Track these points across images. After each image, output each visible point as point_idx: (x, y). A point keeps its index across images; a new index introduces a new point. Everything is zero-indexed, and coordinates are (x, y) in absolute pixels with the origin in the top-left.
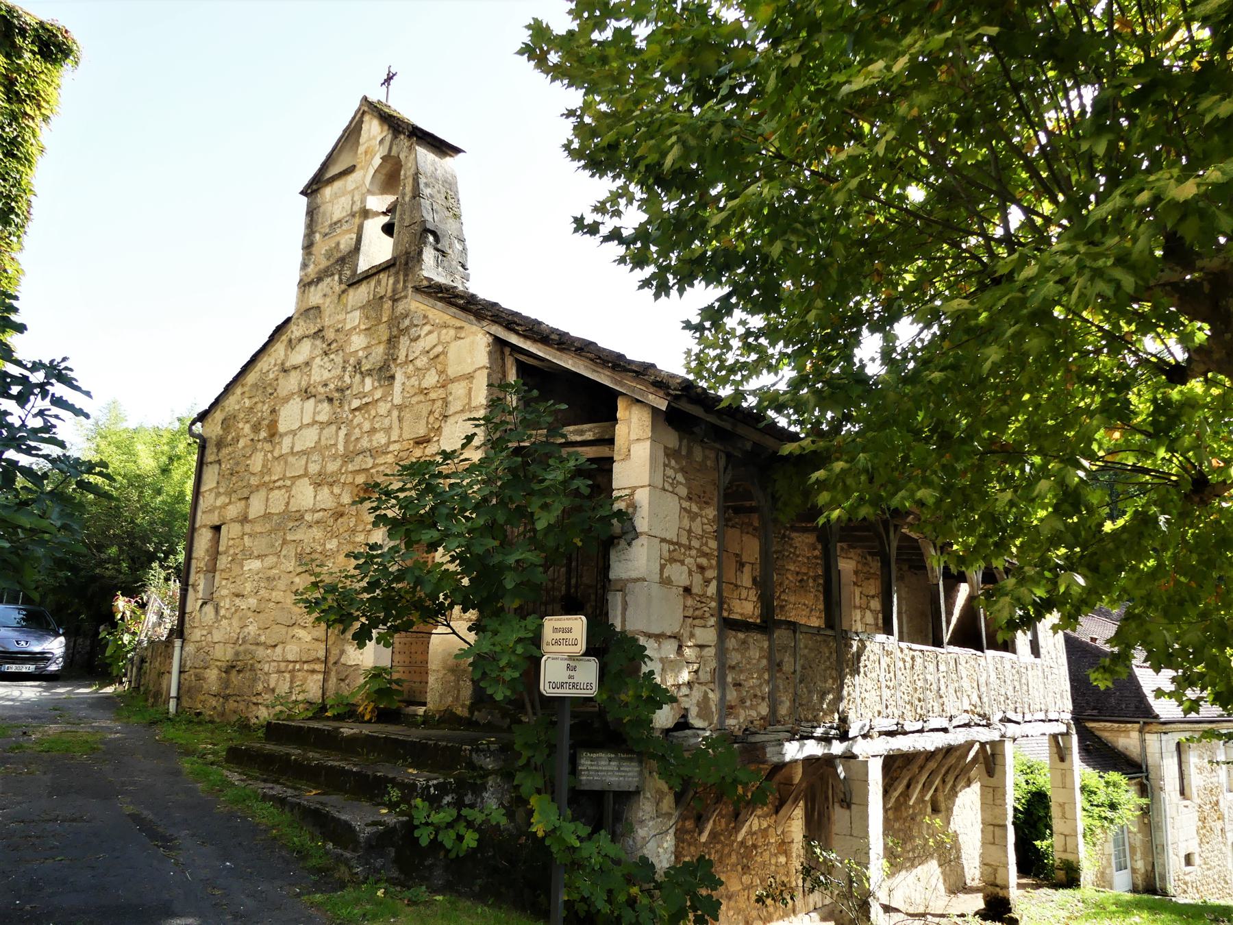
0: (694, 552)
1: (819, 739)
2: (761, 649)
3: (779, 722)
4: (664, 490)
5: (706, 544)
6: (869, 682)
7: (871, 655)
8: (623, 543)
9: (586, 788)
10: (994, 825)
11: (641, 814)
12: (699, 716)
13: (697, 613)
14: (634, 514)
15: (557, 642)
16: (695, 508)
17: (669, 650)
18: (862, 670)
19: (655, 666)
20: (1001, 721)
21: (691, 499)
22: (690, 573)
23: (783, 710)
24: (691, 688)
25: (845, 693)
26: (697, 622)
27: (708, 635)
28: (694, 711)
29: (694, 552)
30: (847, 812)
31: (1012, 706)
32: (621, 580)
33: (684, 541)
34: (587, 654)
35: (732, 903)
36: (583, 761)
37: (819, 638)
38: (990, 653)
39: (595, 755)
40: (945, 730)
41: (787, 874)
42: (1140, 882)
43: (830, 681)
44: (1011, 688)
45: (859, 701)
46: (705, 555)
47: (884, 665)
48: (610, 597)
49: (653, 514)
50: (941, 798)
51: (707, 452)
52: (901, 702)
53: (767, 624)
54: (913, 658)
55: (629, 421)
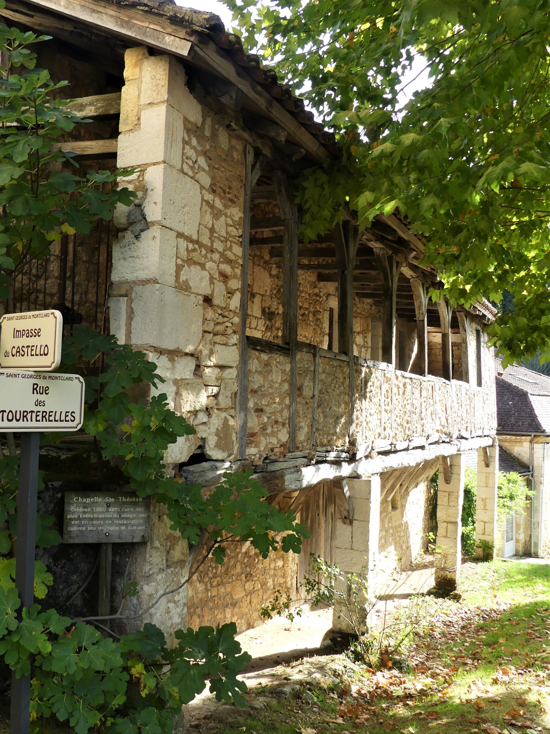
0: (216, 256)
1: (333, 463)
2: (283, 372)
3: (297, 448)
4: (182, 171)
5: (230, 249)
6: (372, 406)
7: (376, 381)
8: (129, 235)
9: (77, 541)
10: (447, 522)
11: (147, 568)
12: (218, 446)
13: (220, 328)
14: (144, 198)
15: (19, 352)
16: (218, 204)
17: (185, 369)
18: (368, 395)
19: (168, 389)
20: (458, 438)
21: (214, 191)
22: (212, 278)
23: (301, 436)
24: (209, 415)
25: (354, 417)
26: (218, 339)
27: (230, 354)
28: (212, 441)
29: (216, 256)
30: (349, 528)
31: (465, 426)
32: (127, 282)
33: (205, 240)
34: (64, 367)
35: (236, 610)
36: (72, 508)
37: (335, 363)
38: (454, 382)
39: (88, 500)
40: (422, 448)
41: (284, 576)
42: (521, 549)
43: (343, 406)
44: (465, 412)
45: (364, 424)
46: (229, 262)
47: (384, 391)
48: (112, 303)
49: (168, 200)
50: (398, 498)
51: (234, 142)
52: (395, 425)
53: (288, 347)
54: (404, 385)
55: (138, 80)
